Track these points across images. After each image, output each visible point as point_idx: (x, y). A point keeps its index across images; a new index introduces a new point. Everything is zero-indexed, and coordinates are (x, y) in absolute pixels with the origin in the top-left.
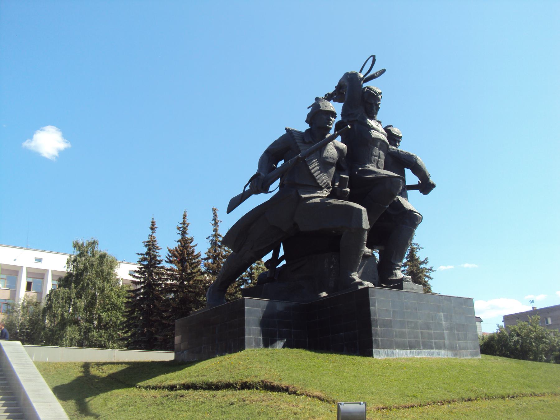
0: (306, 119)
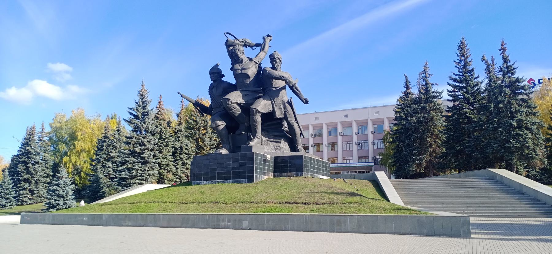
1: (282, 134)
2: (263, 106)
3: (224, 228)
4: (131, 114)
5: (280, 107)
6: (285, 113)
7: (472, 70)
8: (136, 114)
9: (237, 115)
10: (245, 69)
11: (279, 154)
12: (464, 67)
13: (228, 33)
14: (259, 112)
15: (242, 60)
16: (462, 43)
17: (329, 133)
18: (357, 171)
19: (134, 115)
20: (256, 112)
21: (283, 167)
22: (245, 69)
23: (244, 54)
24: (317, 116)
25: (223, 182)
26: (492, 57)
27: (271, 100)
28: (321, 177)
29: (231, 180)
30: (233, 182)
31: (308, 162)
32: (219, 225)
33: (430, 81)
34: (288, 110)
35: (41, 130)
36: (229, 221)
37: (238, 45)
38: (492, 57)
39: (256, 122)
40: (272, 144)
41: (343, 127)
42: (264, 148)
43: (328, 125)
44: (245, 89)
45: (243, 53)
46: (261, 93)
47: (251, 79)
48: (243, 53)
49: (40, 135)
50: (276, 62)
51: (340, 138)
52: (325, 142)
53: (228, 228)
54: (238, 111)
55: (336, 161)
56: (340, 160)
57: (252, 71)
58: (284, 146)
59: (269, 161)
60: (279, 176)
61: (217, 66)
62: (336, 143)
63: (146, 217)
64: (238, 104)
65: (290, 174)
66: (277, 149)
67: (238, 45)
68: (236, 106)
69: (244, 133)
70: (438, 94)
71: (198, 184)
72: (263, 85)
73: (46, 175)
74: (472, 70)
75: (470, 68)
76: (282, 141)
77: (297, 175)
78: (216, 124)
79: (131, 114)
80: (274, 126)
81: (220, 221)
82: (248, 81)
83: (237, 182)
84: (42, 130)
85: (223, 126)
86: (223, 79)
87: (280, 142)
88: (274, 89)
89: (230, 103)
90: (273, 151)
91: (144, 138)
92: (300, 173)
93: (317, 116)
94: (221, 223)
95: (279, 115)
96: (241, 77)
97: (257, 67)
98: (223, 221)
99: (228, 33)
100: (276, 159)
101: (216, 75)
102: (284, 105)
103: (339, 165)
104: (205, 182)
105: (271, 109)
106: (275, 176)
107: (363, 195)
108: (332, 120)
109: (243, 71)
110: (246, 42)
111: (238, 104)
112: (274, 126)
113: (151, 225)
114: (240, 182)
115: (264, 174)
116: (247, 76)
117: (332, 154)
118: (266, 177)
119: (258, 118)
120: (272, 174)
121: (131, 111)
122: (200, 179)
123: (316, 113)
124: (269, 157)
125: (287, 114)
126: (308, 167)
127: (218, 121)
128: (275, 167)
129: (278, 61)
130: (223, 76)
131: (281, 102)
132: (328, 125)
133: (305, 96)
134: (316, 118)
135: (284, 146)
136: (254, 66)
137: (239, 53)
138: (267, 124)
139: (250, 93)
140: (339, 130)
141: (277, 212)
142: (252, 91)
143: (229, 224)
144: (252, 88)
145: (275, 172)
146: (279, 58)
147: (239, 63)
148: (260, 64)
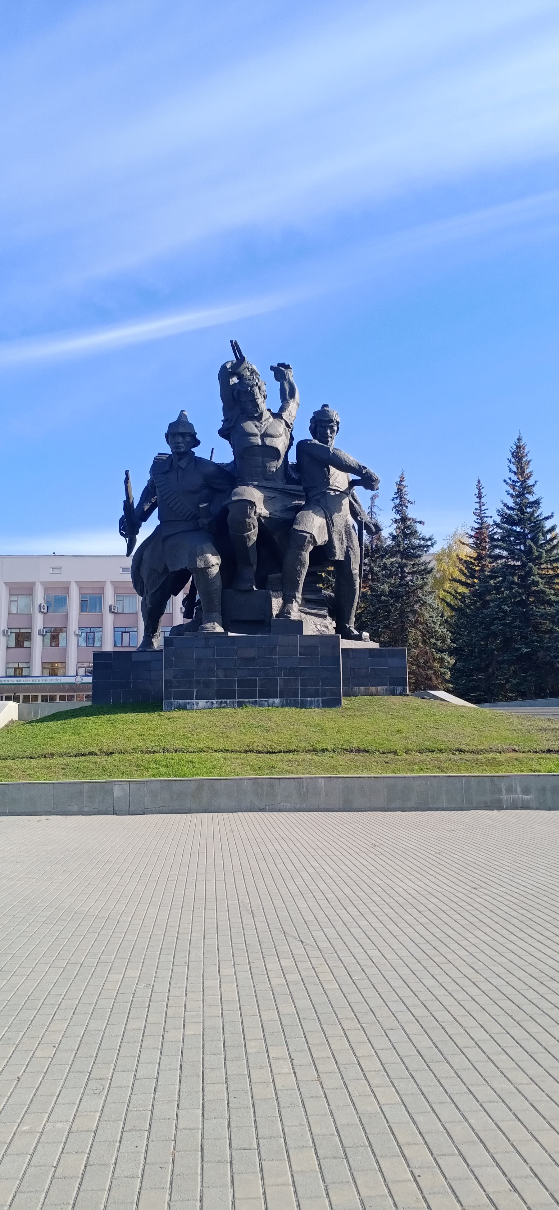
0: (220, 425)
3: (514, 806)
7: (537, 503)
10: (271, 436)
12: (521, 495)
16: (518, 447)
17: (84, 605)
18: (21, 695)
22: (271, 436)
24: (56, 563)
25: (255, 703)
26: (479, 482)
27: (326, 518)
29: (277, 701)
30: (283, 705)
32: (500, 801)
33: (411, 512)
36: (526, 791)
38: (479, 482)
41: (117, 595)
43: (81, 586)
44: (264, 483)
46: (299, 497)
48: (265, 397)
51: (109, 620)
52: (73, 624)
53: (525, 806)
55: (61, 672)
56: (37, 670)
62: (101, 627)
63: (271, 786)
65: (373, 689)
70: (422, 542)
71: (184, 708)
74: (537, 503)
75: (532, 498)
77: (393, 693)
81: (500, 792)
83: (295, 704)
92: (399, 689)
93: (56, 563)
94: (504, 797)
98: (510, 790)
103: (29, 680)
104: (202, 703)
108: (92, 576)
109: (268, 441)
113: (289, 806)
114: (303, 705)
117: (54, 655)
119: (306, 556)
122: (188, 696)
123: (54, 556)
125: (351, 552)
127: (209, 556)
130: (197, 443)
132: (81, 586)
134: (53, 568)
140: (109, 599)
142: (283, 492)
143: (527, 797)
147: (252, 418)
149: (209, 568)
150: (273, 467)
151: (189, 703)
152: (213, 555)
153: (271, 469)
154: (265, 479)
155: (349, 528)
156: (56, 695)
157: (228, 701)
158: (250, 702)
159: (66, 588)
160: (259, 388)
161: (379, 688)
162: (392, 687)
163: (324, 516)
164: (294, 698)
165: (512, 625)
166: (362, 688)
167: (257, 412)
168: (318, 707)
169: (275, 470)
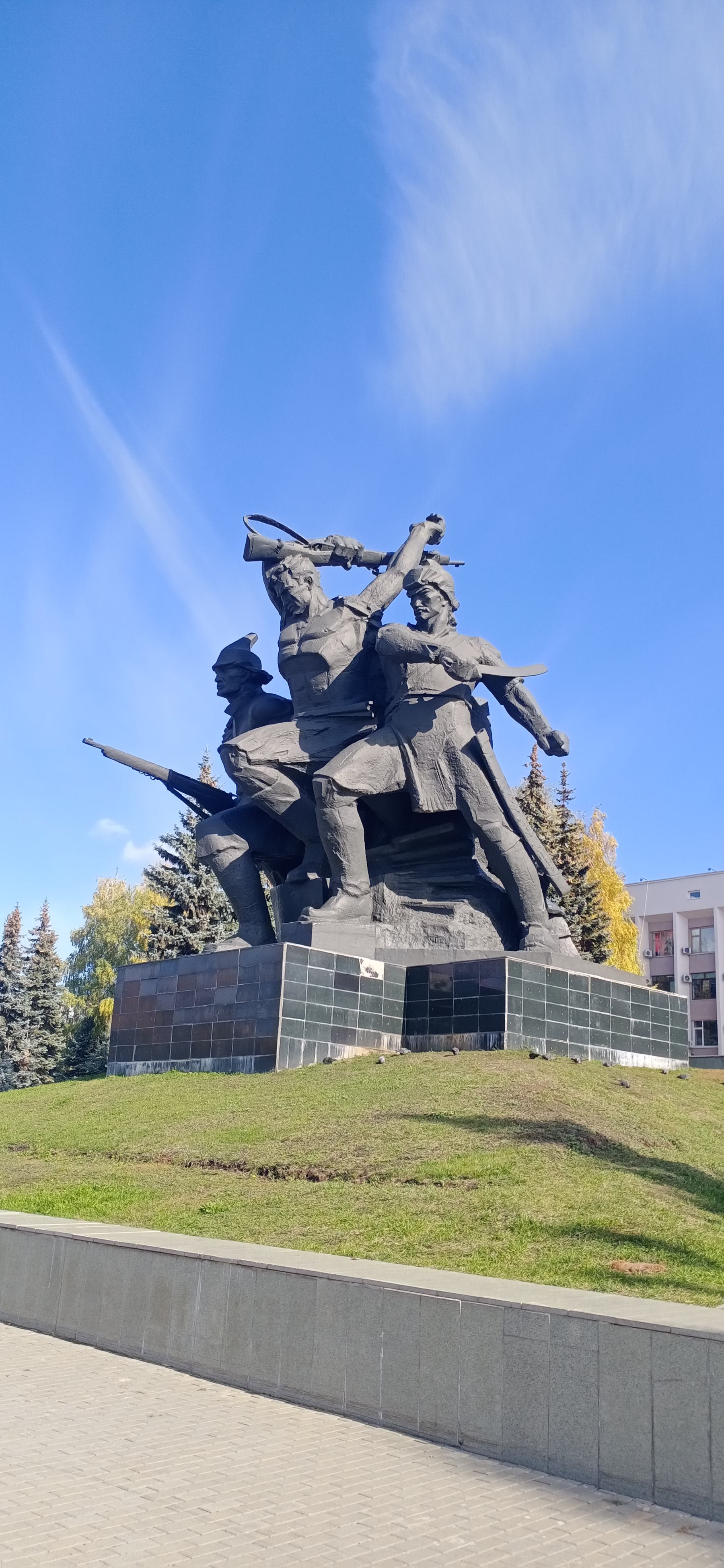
1: (468, 877)
2: (365, 766)
4: (165, 855)
5: (435, 768)
6: (459, 793)
8: (177, 855)
9: (282, 809)
11: (436, 956)
13: (253, 518)
14: (344, 791)
15: (307, 608)
19: (174, 859)
20: (330, 792)
21: (448, 1008)
23: (317, 589)
27: (400, 744)
28: (629, 1059)
29: (208, 1061)
31: (534, 989)
34: (472, 780)
35: (39, 924)
37: (294, 553)
39: (334, 829)
40: (416, 918)
42: (367, 933)
45: (309, 581)
46: (369, 720)
47: (336, 672)
48: (309, 581)
49: (36, 937)
50: (426, 601)
54: (285, 793)
57: (341, 645)
58: (468, 929)
59: (372, 984)
60: (421, 1048)
61: (245, 643)
64: (281, 767)
66: (434, 940)
67: (294, 553)
68: (272, 773)
69: (312, 876)
71: (122, 1073)
72: (375, 691)
73: (45, 1050)
76: (463, 908)
77: (484, 1045)
78: (208, 846)
79: (165, 855)
80: (428, 848)
82: (323, 682)
84: (43, 925)
85: (239, 854)
86: (265, 688)
87: (450, 912)
88: (414, 701)
89: (243, 764)
90: (418, 946)
91: (194, 929)
92: (492, 1036)
95: (429, 799)
96: (302, 665)
97: (363, 627)
99: (253, 518)
100: (417, 977)
101: (233, 672)
102: (453, 762)
104: (139, 1064)
105: (402, 777)
106: (405, 1044)
107: (461, 1136)
110: (337, 546)
111: (281, 767)
112: (428, 848)
115: (343, 1036)
116: (320, 664)
118: (349, 1052)
119: (348, 818)
120: (398, 1038)
121: (166, 847)
124: (372, 967)
125: (466, 794)
126: (532, 1008)
128: (408, 1011)
129: (433, 594)
131: (439, 749)
133: (550, 724)
135: (468, 929)
136: (350, 626)
137: (291, 582)
138: (404, 840)
139: (332, 724)
141: (43, 1208)
144: (342, 706)
145: (408, 1030)
146: (435, 586)
148: (377, 617)
149: (213, 855)
150: (322, 683)
151: (128, 1066)
152: (222, 834)
153: (320, 687)
154: (317, 704)
155: (454, 753)
156: (705, 1044)
157: (163, 1062)
158: (181, 1064)
159: (668, 919)
160: (290, 573)
161: (466, 1035)
162: (483, 1034)
163: (395, 741)
164: (655, 1054)
165: (176, 866)
166: (443, 1037)
167: (298, 607)
168: (250, 1072)
169: (326, 687)
